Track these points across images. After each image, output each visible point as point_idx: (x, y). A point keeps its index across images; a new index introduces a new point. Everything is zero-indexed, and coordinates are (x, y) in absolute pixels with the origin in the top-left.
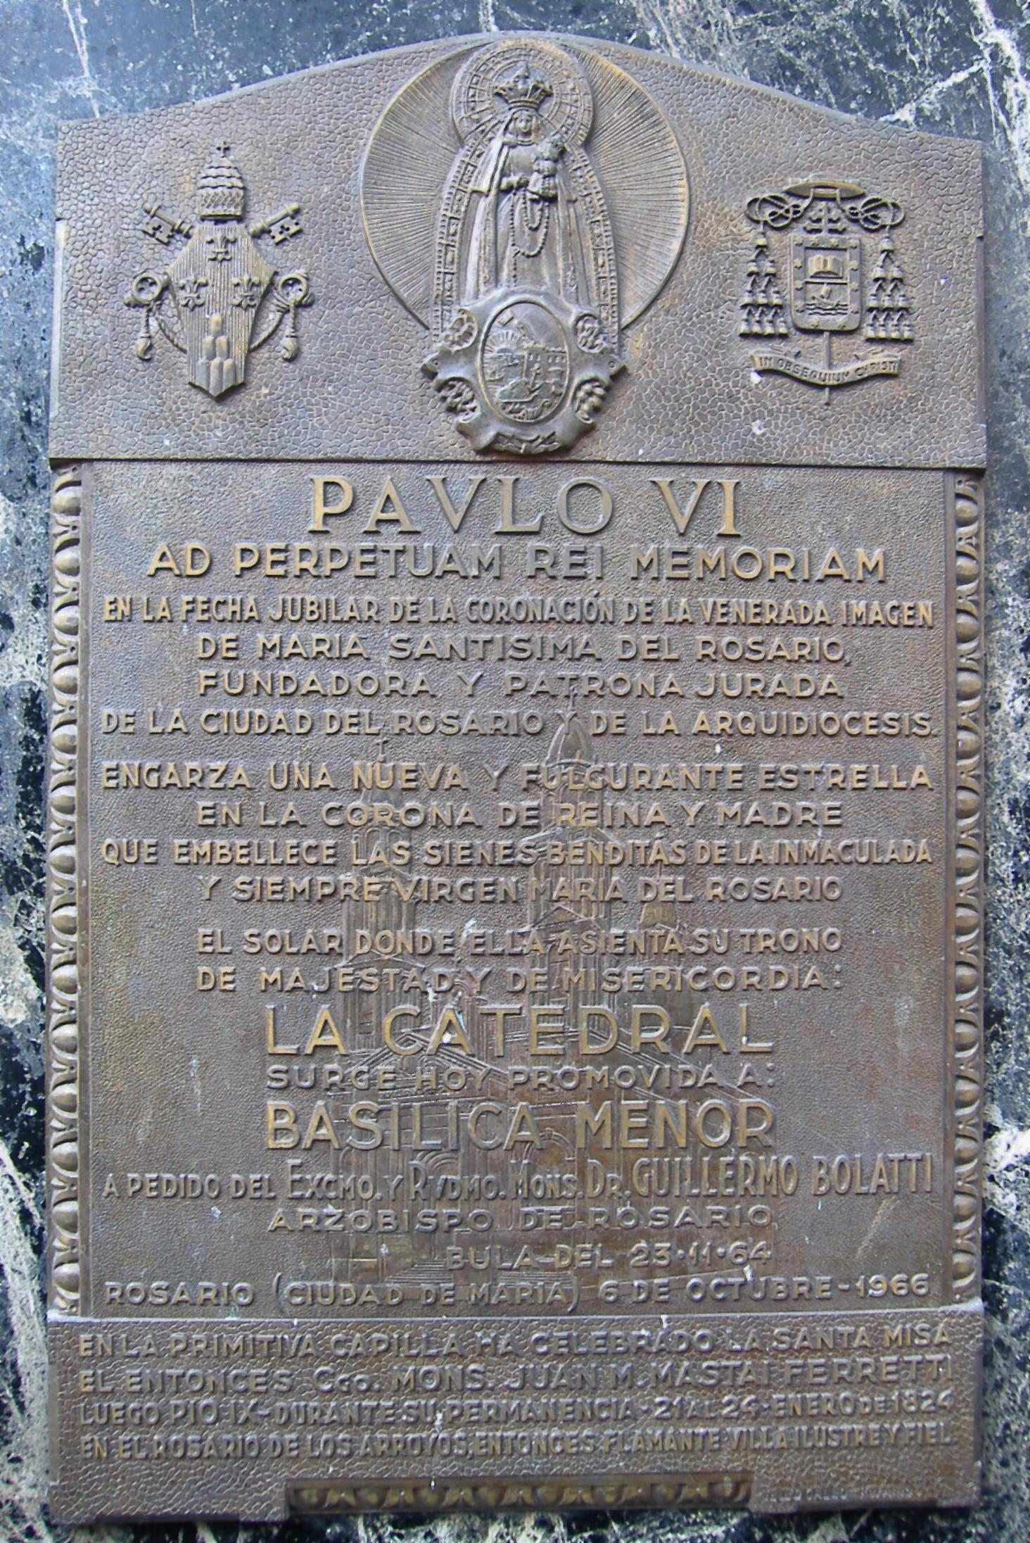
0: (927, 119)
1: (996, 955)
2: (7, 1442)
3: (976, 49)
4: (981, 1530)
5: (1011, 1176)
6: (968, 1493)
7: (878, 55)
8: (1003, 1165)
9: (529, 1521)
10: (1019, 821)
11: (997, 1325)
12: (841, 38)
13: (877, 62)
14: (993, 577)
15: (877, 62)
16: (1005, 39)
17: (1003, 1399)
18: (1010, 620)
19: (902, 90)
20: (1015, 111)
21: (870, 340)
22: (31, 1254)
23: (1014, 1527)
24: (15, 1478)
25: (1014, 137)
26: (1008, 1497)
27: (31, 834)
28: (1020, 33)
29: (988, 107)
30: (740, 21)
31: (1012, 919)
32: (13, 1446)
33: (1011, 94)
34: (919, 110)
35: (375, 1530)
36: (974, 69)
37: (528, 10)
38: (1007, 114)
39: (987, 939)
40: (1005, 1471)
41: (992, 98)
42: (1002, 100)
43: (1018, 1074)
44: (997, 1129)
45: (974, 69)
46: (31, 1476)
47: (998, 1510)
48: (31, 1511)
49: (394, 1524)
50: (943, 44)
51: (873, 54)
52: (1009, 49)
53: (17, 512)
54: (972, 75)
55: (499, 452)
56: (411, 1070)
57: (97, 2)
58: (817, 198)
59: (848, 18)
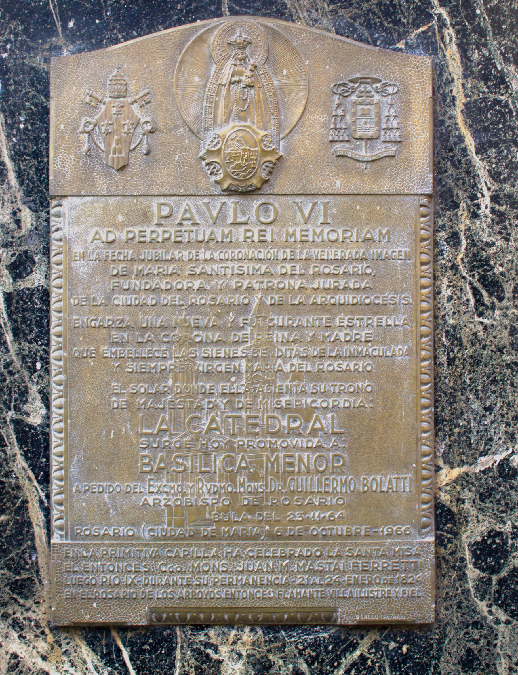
0: (410, 47)
1: (440, 396)
2: (34, 595)
3: (431, 15)
4: (437, 637)
5: (448, 488)
6: (431, 618)
7: (389, 20)
8: (444, 483)
9: (247, 629)
10: (450, 340)
11: (442, 550)
12: (374, 13)
13: (389, 23)
14: (438, 238)
15: (389, 23)
16: (443, 12)
17: (446, 582)
18: (445, 256)
19: (399, 35)
20: (448, 41)
21: (384, 142)
22: (43, 518)
23: (451, 636)
24: (37, 610)
25: (447, 54)
26: (448, 623)
27: (43, 347)
28: (450, 9)
29: (436, 41)
30: (331, 7)
31: (447, 380)
32: (36, 597)
33: (446, 34)
34: (407, 43)
35: (184, 632)
36: (430, 24)
37: (241, 5)
38: (444, 43)
39: (436, 389)
40: (447, 612)
41: (438, 38)
42: (442, 38)
43: (450, 445)
44: (441, 468)
45: (430, 24)
46: (43, 609)
47: (445, 629)
48: (43, 624)
49: (192, 630)
50: (417, 15)
51: (387, 20)
52: (445, 16)
53: (36, 217)
54: (430, 27)
55: (231, 191)
56: (197, 440)
57: (411, 674)
58: (361, 83)
59: (377, 5)
